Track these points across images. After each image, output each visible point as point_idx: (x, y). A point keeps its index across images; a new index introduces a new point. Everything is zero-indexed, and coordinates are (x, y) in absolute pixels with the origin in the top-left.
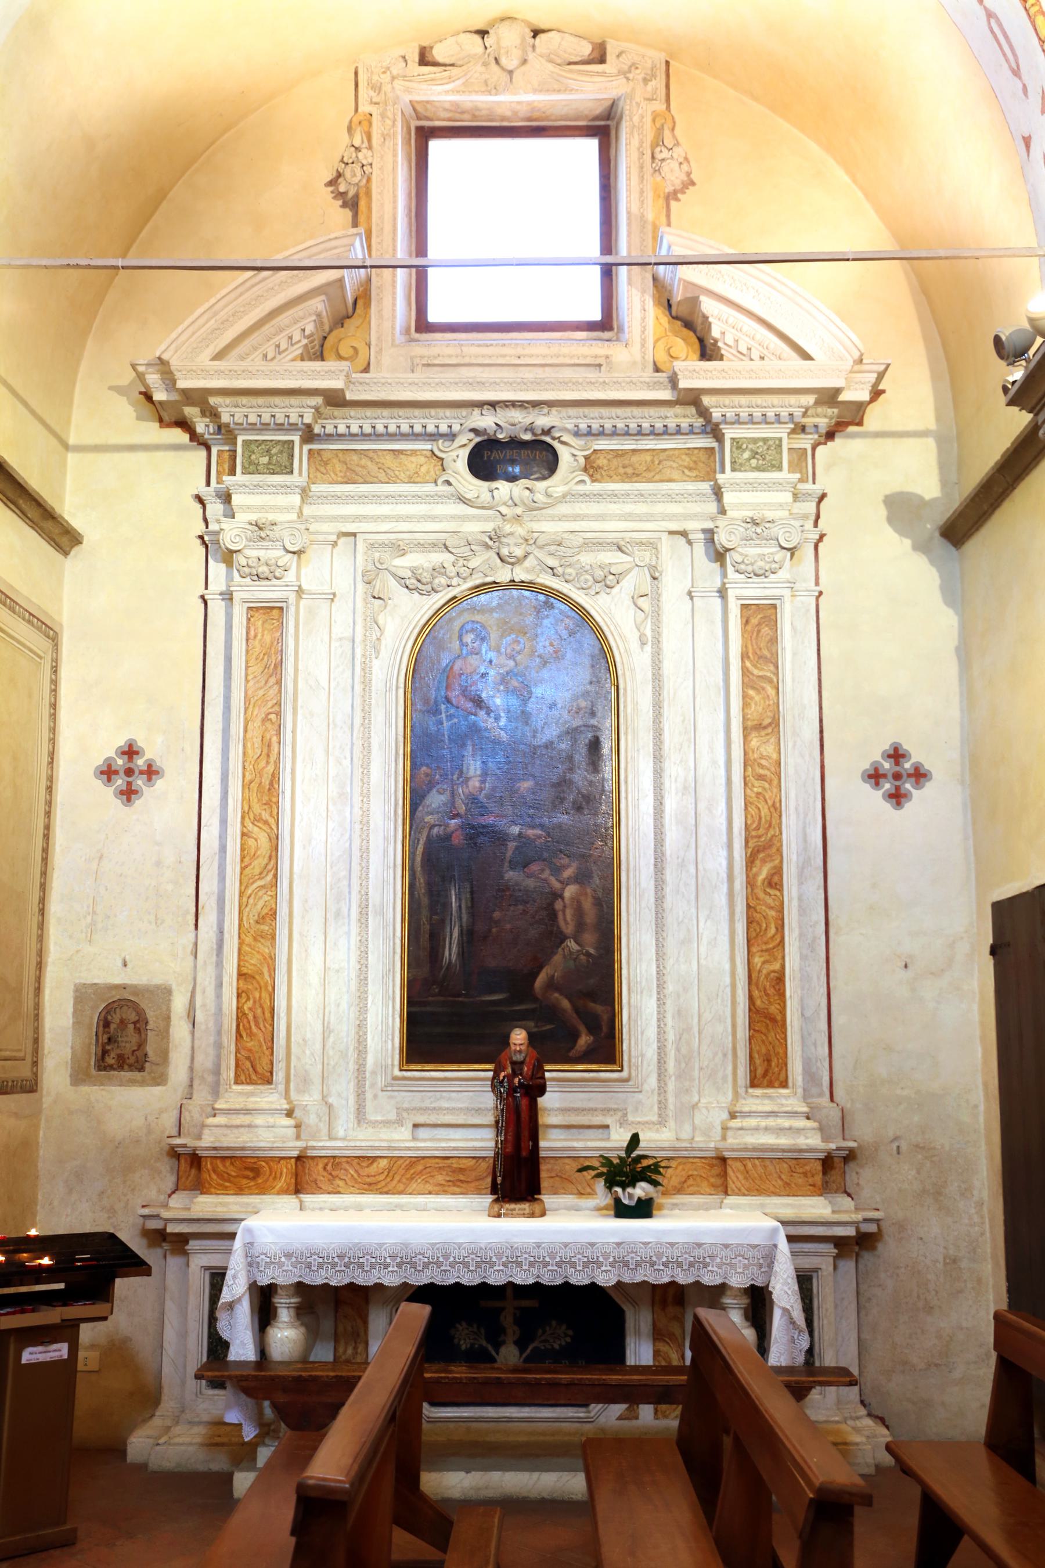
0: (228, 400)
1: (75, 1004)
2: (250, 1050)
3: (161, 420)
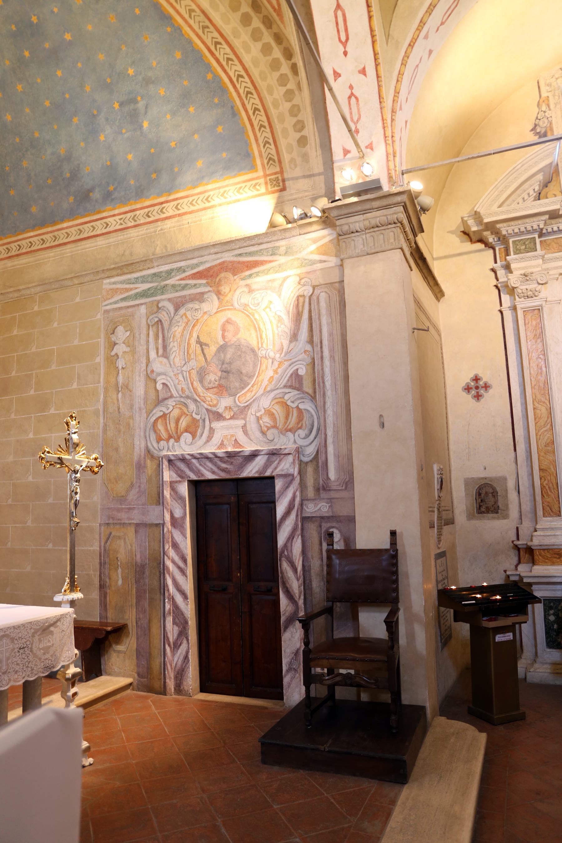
0: (505, 224)
1: (465, 486)
2: (549, 502)
3: (471, 241)
